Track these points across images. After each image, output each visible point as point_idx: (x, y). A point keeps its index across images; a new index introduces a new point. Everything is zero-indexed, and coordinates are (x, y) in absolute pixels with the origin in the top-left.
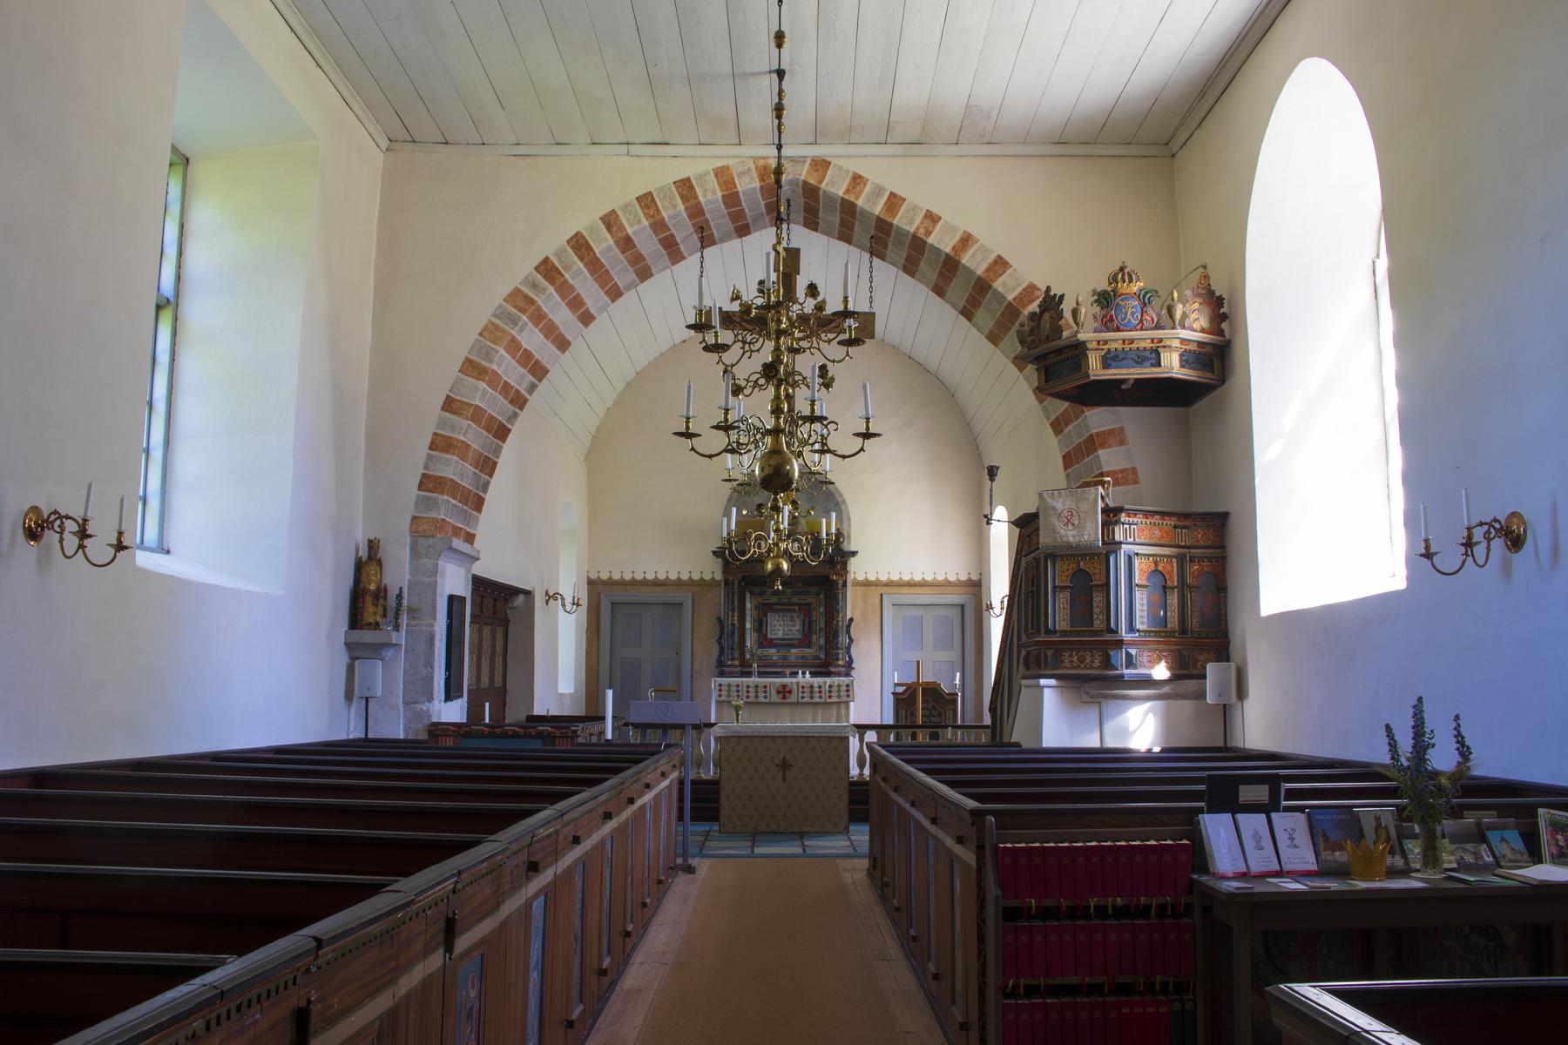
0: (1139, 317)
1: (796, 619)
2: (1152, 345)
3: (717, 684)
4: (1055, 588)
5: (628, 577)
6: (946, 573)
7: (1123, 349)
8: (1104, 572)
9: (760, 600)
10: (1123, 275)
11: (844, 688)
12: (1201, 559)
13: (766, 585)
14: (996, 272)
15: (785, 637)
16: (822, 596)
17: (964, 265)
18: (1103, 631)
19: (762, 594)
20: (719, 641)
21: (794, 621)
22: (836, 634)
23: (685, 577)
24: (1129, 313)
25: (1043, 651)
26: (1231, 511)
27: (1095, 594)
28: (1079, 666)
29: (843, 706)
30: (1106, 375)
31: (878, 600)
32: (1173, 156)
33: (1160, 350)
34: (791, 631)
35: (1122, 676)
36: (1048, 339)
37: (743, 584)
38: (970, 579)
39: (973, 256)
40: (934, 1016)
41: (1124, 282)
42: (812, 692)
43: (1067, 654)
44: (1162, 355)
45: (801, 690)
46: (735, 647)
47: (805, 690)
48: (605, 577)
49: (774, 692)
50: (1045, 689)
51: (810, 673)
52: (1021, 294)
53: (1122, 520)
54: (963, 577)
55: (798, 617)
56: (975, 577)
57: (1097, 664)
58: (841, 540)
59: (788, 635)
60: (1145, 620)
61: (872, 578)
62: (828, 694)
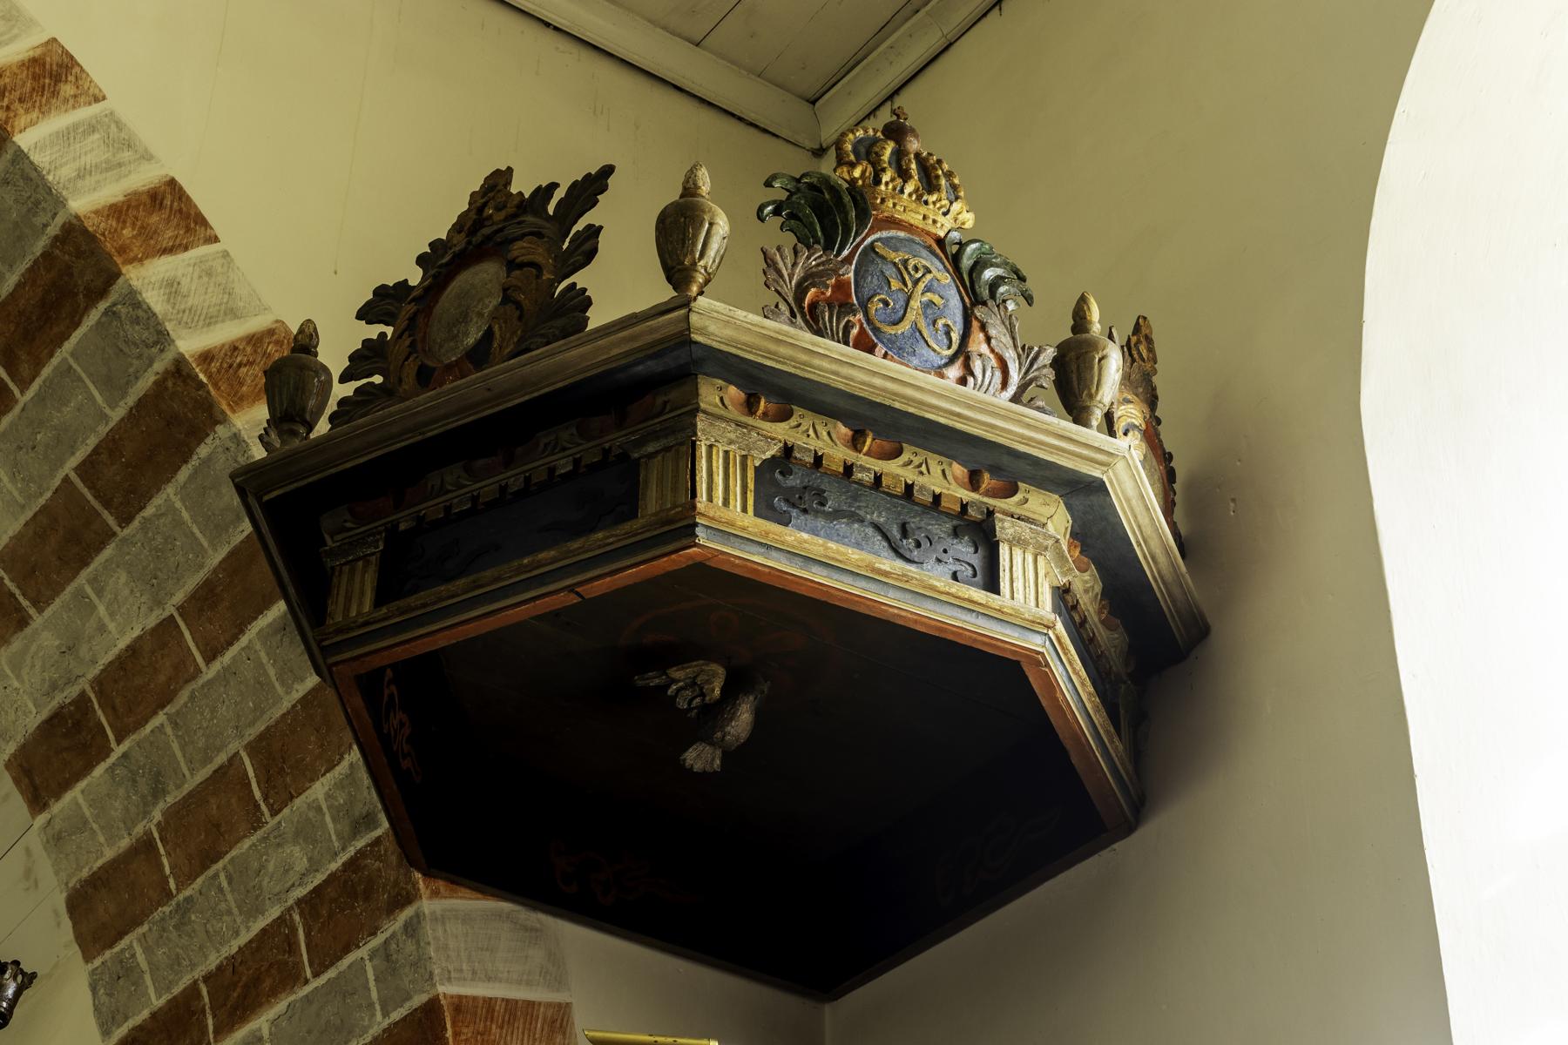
0: (955, 337)
2: (966, 495)
10: (899, 154)
24: (915, 304)
33: (1005, 528)
40: (961, 332)
44: (1004, 550)
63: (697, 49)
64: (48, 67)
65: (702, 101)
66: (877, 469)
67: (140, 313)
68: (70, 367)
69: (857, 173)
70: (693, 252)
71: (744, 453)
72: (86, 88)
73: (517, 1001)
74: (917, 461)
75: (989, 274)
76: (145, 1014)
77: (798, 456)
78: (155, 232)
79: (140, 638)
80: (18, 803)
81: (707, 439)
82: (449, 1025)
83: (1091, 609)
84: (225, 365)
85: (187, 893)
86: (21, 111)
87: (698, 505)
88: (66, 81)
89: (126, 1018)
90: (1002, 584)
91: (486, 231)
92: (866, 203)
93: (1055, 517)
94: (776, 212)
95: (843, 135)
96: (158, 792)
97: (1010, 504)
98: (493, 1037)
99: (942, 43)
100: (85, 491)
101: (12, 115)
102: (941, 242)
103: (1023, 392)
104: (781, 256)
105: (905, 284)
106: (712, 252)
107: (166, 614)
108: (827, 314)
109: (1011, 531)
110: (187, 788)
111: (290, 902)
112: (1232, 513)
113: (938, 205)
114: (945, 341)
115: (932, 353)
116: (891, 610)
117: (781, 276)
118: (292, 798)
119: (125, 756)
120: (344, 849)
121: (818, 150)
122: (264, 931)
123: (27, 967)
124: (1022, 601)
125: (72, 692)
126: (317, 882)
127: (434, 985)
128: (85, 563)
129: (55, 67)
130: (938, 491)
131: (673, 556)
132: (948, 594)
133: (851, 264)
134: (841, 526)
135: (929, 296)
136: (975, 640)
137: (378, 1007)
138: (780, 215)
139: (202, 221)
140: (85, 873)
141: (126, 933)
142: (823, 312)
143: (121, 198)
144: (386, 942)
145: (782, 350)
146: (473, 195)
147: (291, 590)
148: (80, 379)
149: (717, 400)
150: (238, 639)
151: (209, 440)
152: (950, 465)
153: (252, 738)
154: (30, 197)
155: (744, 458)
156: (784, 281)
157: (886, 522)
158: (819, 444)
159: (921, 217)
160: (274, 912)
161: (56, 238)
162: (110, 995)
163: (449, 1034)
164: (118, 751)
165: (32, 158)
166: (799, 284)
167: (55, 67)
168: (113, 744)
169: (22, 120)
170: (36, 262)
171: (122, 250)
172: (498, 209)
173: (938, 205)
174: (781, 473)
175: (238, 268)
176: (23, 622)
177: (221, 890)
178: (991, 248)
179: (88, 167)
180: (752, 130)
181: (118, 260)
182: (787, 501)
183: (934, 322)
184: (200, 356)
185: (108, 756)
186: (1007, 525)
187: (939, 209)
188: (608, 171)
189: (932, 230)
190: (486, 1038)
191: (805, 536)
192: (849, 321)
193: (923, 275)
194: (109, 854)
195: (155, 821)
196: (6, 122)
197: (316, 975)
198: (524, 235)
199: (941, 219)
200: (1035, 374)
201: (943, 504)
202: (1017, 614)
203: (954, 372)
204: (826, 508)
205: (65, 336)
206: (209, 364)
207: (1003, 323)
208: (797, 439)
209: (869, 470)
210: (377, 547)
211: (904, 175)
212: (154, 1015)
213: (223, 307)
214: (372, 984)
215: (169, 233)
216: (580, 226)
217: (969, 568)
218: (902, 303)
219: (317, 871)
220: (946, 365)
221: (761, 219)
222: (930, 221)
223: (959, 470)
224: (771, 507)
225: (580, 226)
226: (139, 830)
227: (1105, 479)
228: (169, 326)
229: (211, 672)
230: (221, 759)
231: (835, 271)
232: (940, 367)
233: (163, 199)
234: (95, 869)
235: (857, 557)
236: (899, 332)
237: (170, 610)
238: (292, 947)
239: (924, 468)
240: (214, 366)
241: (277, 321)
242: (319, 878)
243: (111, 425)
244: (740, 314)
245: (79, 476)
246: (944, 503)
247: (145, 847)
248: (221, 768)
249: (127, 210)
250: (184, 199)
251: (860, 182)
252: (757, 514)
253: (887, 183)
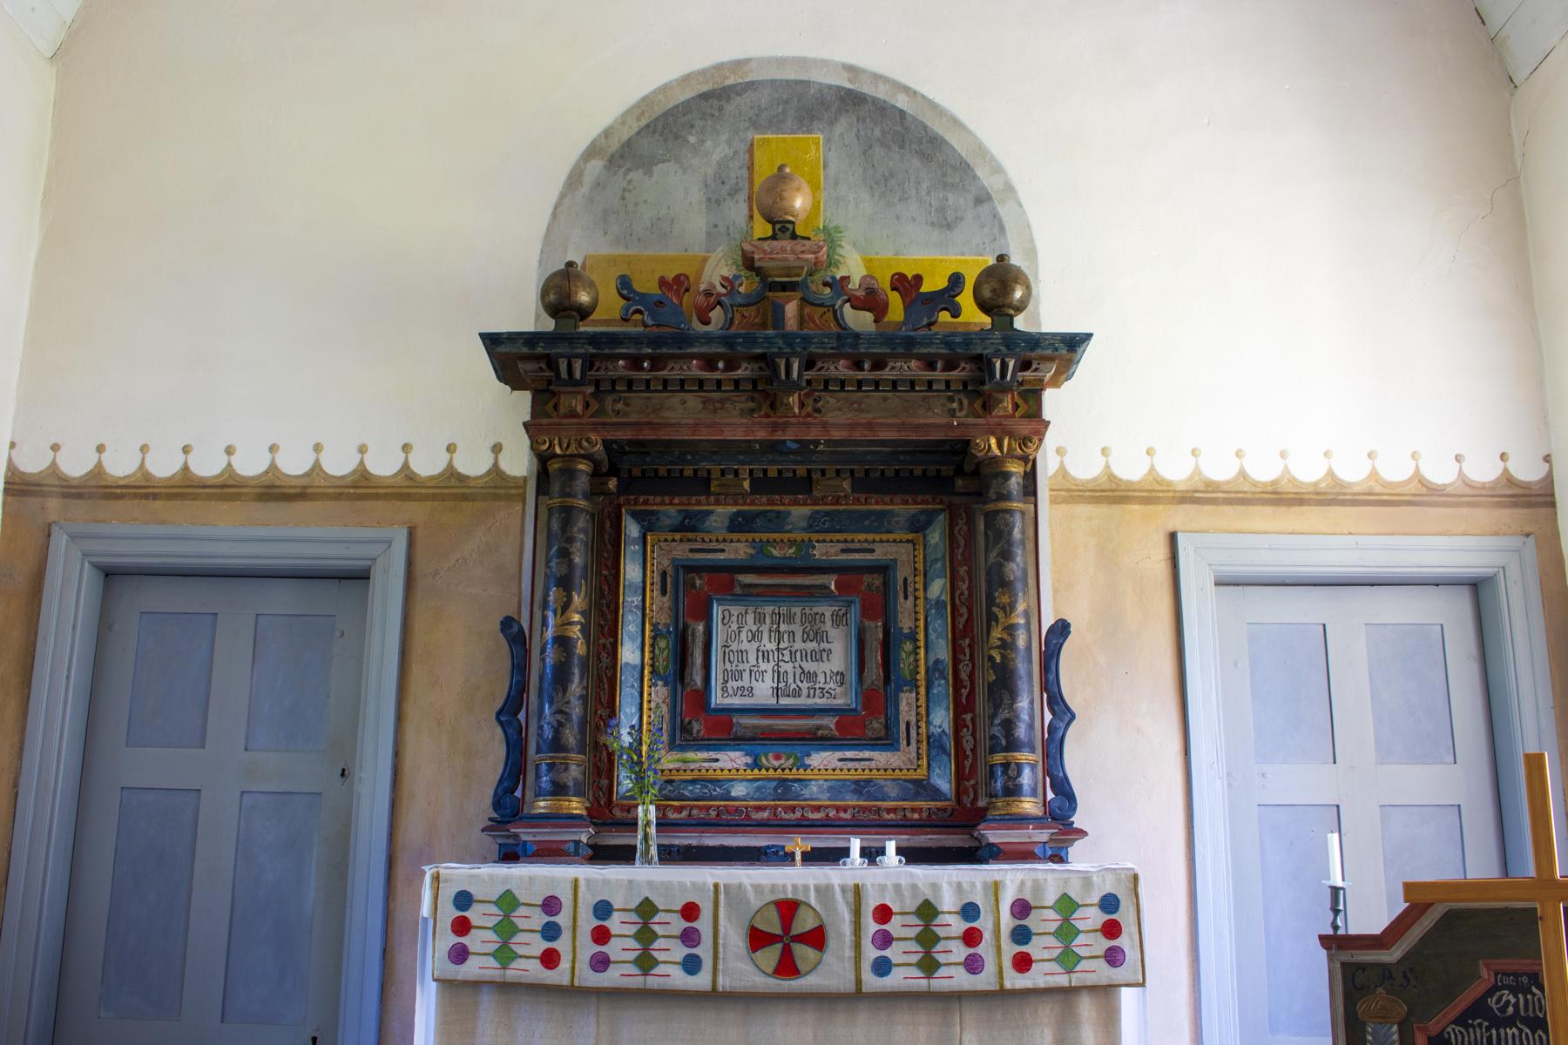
1: (834, 633)
3: (448, 893)
5: (164, 467)
6: (1414, 456)
9: (681, 551)
11: (1092, 918)
13: (708, 493)
15: (784, 701)
16: (936, 536)
19: (689, 525)
20: (509, 713)
21: (819, 636)
22: (1004, 684)
23: (384, 466)
29: (1086, 1008)
31: (1160, 552)
34: (811, 676)
37: (612, 484)
38: (1508, 479)
42: (928, 939)
45: (871, 927)
46: (570, 737)
47: (894, 926)
48: (75, 466)
49: (734, 938)
51: (899, 851)
54: (1484, 471)
55: (838, 620)
56: (1528, 471)
58: (1018, 294)
59: (797, 693)
61: (1131, 470)
62: (1010, 949)
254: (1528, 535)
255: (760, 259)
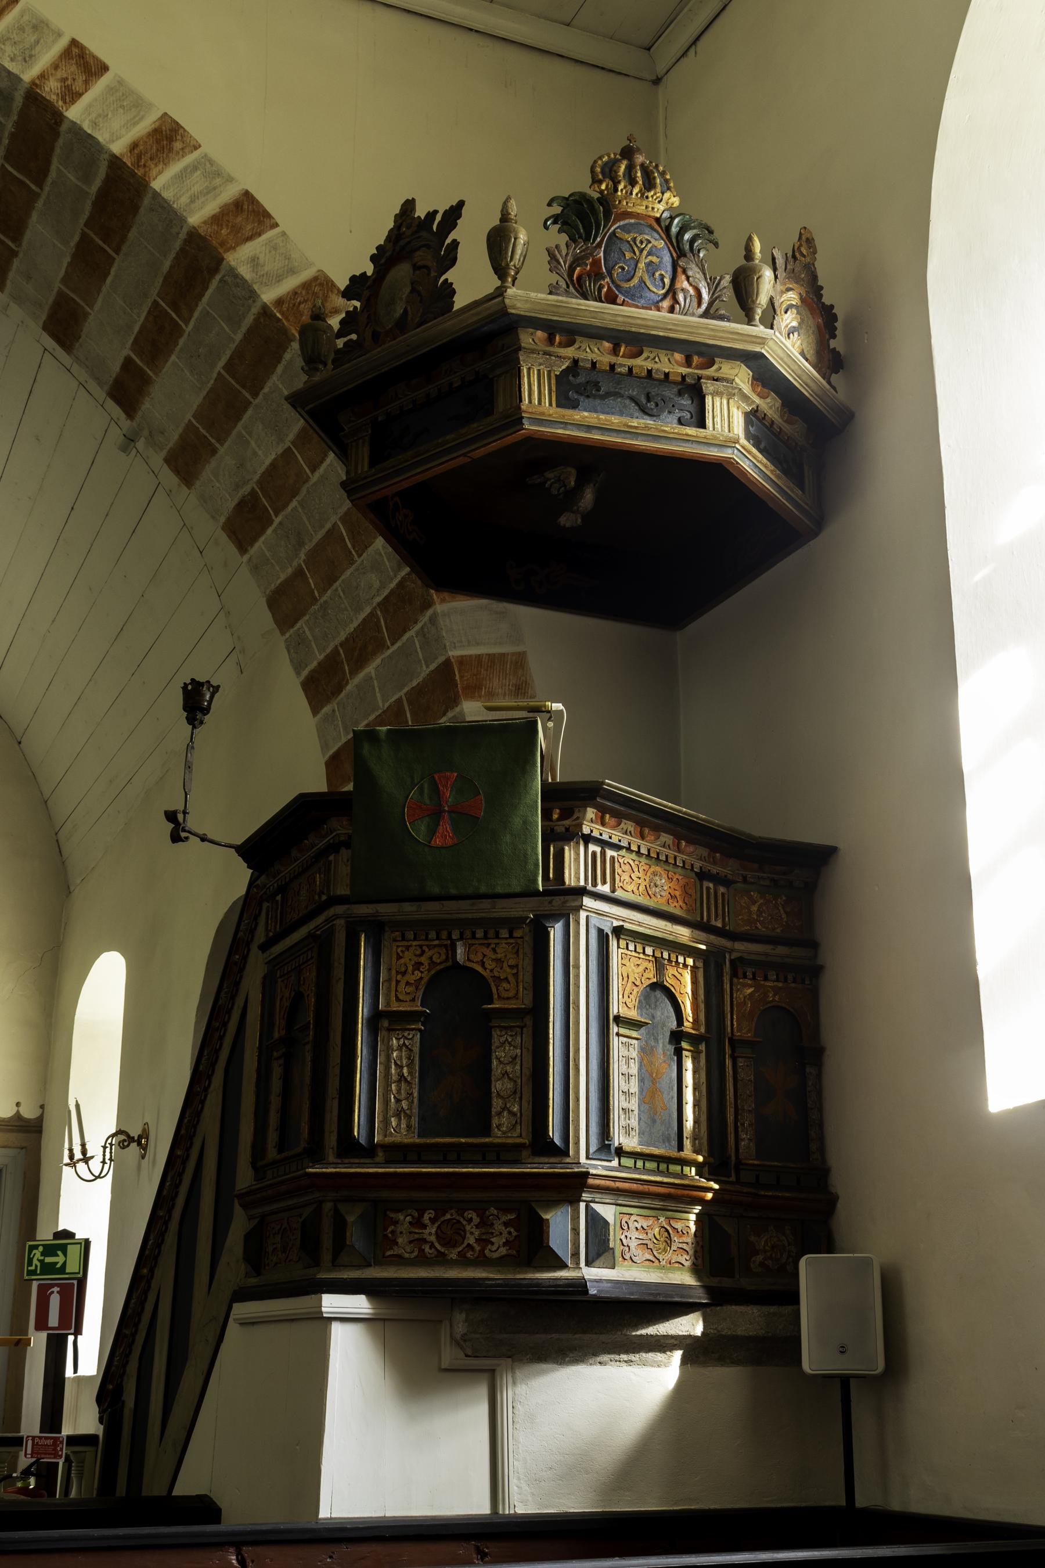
0: (667, 281)
2: (684, 370)
4: (376, 1018)
7: (612, 367)
8: (527, 975)
10: (630, 168)
12: (762, 967)
14: (236, 230)
17: (156, 195)
18: (522, 1146)
24: (642, 265)
25: (328, 1206)
26: (841, 846)
27: (497, 1037)
28: (443, 1254)
30: (565, 425)
32: (657, 81)
33: (708, 387)
35: (581, 1286)
36: (402, 325)
38: (18, 1116)
39: (181, 176)
41: (633, 182)
43: (404, 1219)
44: (709, 400)
50: (336, 1328)
52: (295, 293)
53: (586, 830)
56: (29, 1112)
57: (498, 1248)
60: (634, 1122)
63: (569, 28)
64: (164, 133)
65: (577, 61)
66: (629, 364)
67: (238, 280)
68: (208, 312)
69: (603, 187)
70: (506, 258)
71: (548, 369)
72: (188, 141)
73: (494, 655)
74: (652, 356)
75: (687, 236)
76: (315, 664)
77: (582, 364)
78: (240, 228)
79: (275, 459)
80: (232, 549)
81: (527, 365)
82: (457, 673)
83: (775, 416)
84: (291, 305)
85: (324, 598)
86: (153, 166)
87: (522, 407)
88: (176, 140)
89: (306, 666)
90: (707, 421)
91: (402, 243)
92: (609, 206)
93: (742, 376)
94: (555, 222)
95: (595, 162)
96: (301, 544)
97: (711, 372)
98: (482, 676)
99: (720, 6)
100: (230, 379)
101: (147, 169)
102: (658, 220)
103: (712, 306)
104: (558, 251)
105: (634, 253)
106: (517, 257)
107: (286, 446)
108: (587, 282)
109: (711, 388)
110: (315, 541)
111: (374, 604)
112: (866, 341)
113: (655, 197)
114: (661, 284)
115: (653, 294)
116: (641, 447)
117: (559, 263)
118: (366, 548)
119: (280, 523)
120: (395, 576)
121: (656, 80)
122: (364, 620)
123: (214, 683)
124: (720, 430)
125: (246, 489)
126: (385, 594)
127: (447, 652)
128: (238, 418)
129: (168, 132)
130: (667, 371)
131: (513, 435)
132: (673, 433)
133: (601, 248)
134: (610, 401)
135: (650, 258)
136: (692, 456)
137: (423, 662)
138: (557, 223)
139: (267, 215)
140: (273, 587)
141: (299, 620)
142: (585, 281)
143: (218, 210)
144: (422, 628)
145: (562, 310)
146: (396, 216)
147: (335, 448)
148: (214, 318)
149: (531, 340)
150: (325, 460)
151: (289, 350)
152: (673, 355)
153: (341, 514)
154: (166, 218)
155: (549, 372)
156: (561, 266)
157: (637, 394)
158: (594, 356)
159: (644, 208)
160: (368, 610)
161: (185, 240)
162: (297, 653)
163: (457, 677)
164: (277, 521)
165: (163, 195)
166: (570, 266)
167: (168, 132)
168: (274, 517)
169: (154, 172)
170: (177, 253)
171: (222, 244)
172: (408, 228)
173: (655, 197)
174: (573, 376)
175: (292, 241)
176: (214, 451)
177: (339, 596)
178: (690, 217)
179: (196, 193)
180: (612, 75)
181: (221, 250)
182: (577, 392)
183: (653, 274)
184: (276, 302)
185: (272, 523)
186: (708, 385)
187: (655, 200)
188: (461, 204)
189: (652, 214)
190: (478, 677)
191: (586, 414)
192: (601, 284)
193: (646, 245)
194: (283, 577)
195: (302, 559)
196: (145, 175)
197: (393, 644)
198: (420, 247)
199: (657, 206)
200: (720, 293)
201: (670, 378)
202: (715, 438)
203: (666, 304)
204: (601, 393)
205: (201, 296)
206: (282, 307)
207: (697, 265)
208: (578, 355)
209: (624, 365)
210: (368, 432)
211: (633, 182)
212: (319, 664)
213: (286, 268)
214: (419, 650)
215: (249, 227)
216: (448, 241)
217: (688, 414)
218: (633, 266)
219: (384, 588)
220: (662, 300)
221: (546, 228)
222: (650, 209)
223: (678, 357)
224: (567, 398)
225: (448, 241)
226: (295, 563)
227: (763, 351)
228: (256, 287)
229: (315, 478)
230: (328, 526)
231: (591, 254)
232: (658, 302)
233: (242, 206)
234: (277, 585)
235: (617, 421)
236: (632, 285)
237: (288, 444)
238: (379, 629)
239: (657, 359)
240: (285, 307)
241: (319, 271)
242: (386, 592)
243: (236, 343)
244: (533, 295)
245: (225, 371)
246: (671, 378)
247: (299, 573)
248: (329, 530)
249: (222, 217)
250: (255, 203)
251: (606, 192)
252: (558, 406)
253: (622, 190)
254: (22, 1148)
255: (655, 996)
